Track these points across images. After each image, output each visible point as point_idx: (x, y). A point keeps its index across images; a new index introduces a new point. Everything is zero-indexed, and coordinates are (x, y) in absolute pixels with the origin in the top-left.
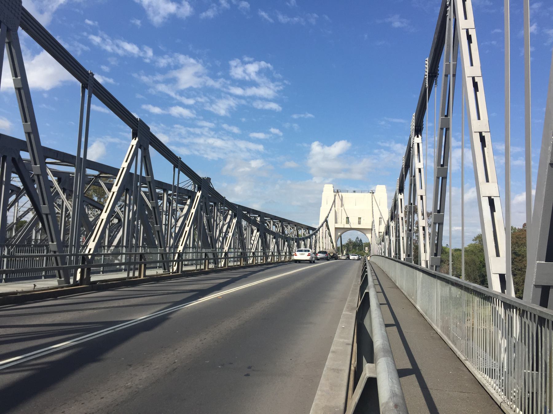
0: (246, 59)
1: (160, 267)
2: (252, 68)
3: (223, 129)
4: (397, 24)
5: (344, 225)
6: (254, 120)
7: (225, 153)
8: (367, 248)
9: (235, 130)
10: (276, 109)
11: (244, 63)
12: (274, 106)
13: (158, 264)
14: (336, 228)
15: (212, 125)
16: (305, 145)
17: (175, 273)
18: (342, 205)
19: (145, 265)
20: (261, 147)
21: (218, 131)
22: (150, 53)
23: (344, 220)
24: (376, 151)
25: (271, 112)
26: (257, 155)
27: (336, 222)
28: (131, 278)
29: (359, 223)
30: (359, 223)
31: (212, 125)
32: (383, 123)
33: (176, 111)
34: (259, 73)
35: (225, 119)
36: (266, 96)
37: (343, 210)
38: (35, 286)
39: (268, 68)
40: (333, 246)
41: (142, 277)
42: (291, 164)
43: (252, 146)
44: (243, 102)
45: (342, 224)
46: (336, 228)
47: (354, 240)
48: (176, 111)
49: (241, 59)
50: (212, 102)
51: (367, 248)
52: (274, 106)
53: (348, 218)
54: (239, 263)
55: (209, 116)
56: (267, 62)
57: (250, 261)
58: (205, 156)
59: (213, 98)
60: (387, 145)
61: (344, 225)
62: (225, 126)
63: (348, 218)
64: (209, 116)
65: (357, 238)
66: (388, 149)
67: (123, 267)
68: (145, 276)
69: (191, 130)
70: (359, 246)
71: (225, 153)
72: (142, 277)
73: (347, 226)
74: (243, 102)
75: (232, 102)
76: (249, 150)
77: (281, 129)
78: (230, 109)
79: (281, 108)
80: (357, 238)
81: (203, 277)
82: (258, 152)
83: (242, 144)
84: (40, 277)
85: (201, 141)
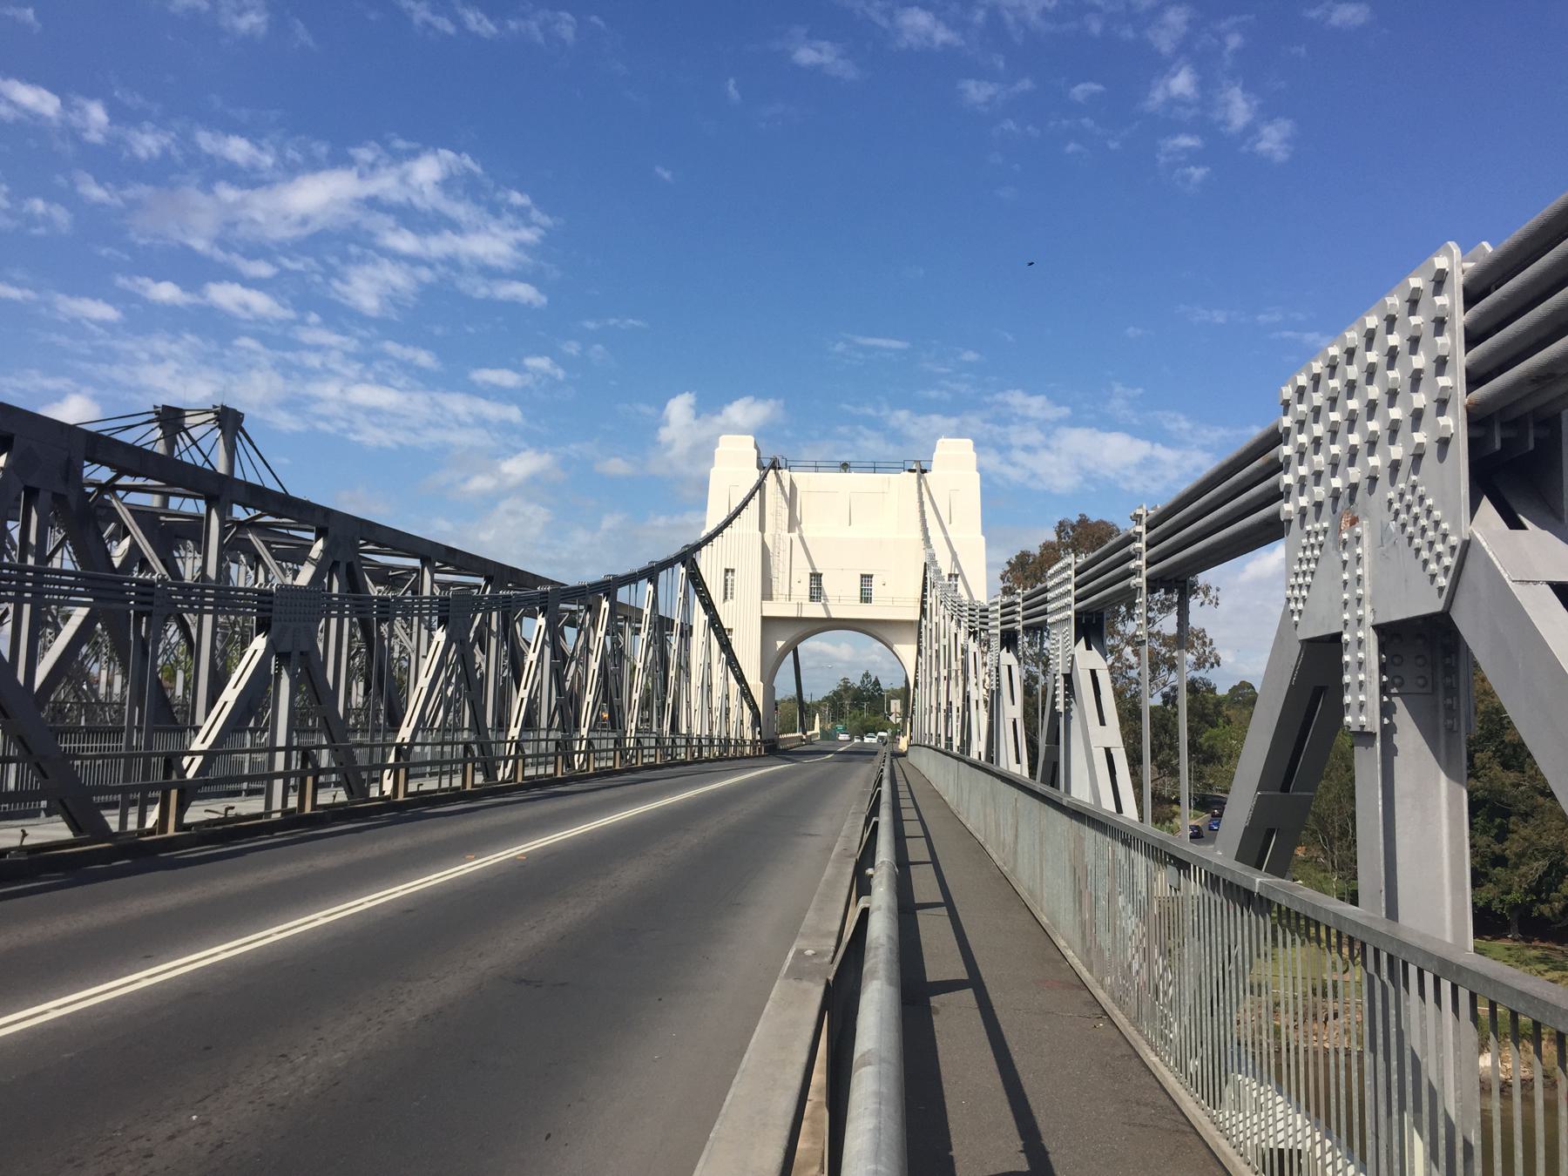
0: (400, 144)
1: (337, 784)
2: (427, 170)
3: (383, 356)
4: (806, 56)
5: (800, 605)
6: (471, 330)
7: (413, 430)
8: (896, 705)
9: (424, 358)
10: (530, 303)
11: (398, 157)
12: (522, 291)
13: (245, 786)
14: (766, 621)
15: (352, 345)
16: (645, 409)
17: (151, 832)
18: (793, 523)
19: (407, 771)
20: (514, 413)
21: (368, 361)
22: (97, 113)
23: (803, 588)
24: (843, 430)
25: (513, 307)
26: (511, 439)
27: (767, 594)
28: (445, 790)
29: (866, 598)
30: (866, 598)
31: (352, 345)
32: (840, 347)
33: (225, 295)
34: (447, 184)
35: (383, 326)
36: (492, 261)
37: (797, 543)
38: (25, 835)
39: (469, 173)
40: (746, 693)
41: (171, 832)
42: (617, 466)
43: (491, 410)
44: (425, 274)
45: (792, 602)
46: (766, 621)
47: (856, 681)
48: (225, 295)
49: (385, 144)
50: (330, 273)
51: (896, 705)
52: (522, 291)
53: (816, 577)
54: (550, 770)
55: (339, 316)
56: (458, 152)
57: (503, 773)
58: (353, 437)
59: (333, 260)
60: (870, 411)
61: (800, 605)
62: (391, 347)
63: (816, 577)
64: (339, 316)
65: (867, 675)
66: (875, 424)
67: (334, 777)
68: (180, 826)
69: (289, 355)
70: (871, 698)
71: (413, 430)
72: (171, 832)
73: (814, 611)
74: (425, 274)
75: (396, 277)
76: (482, 422)
77: (560, 359)
78: (392, 298)
79: (544, 300)
80: (867, 675)
81: (536, 792)
82: (506, 427)
83: (458, 404)
84: (35, 814)
85: (330, 390)
